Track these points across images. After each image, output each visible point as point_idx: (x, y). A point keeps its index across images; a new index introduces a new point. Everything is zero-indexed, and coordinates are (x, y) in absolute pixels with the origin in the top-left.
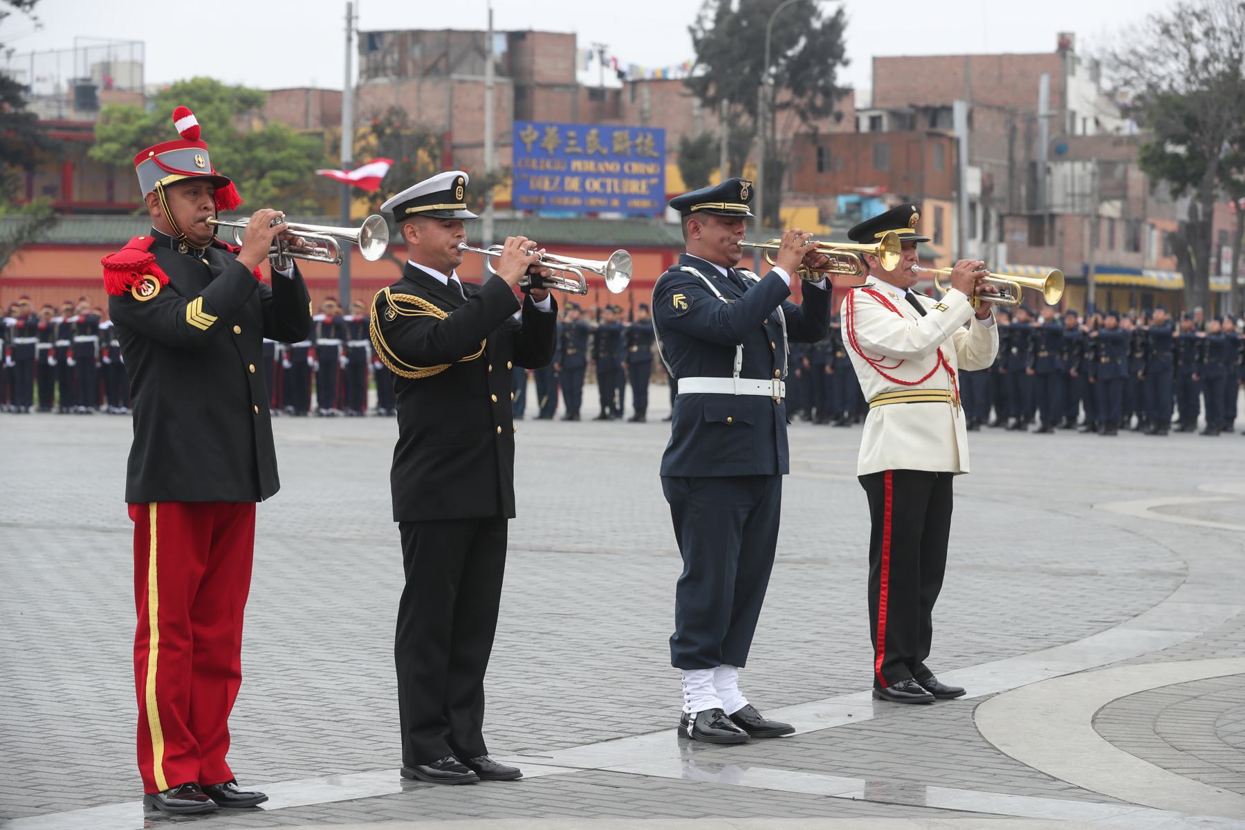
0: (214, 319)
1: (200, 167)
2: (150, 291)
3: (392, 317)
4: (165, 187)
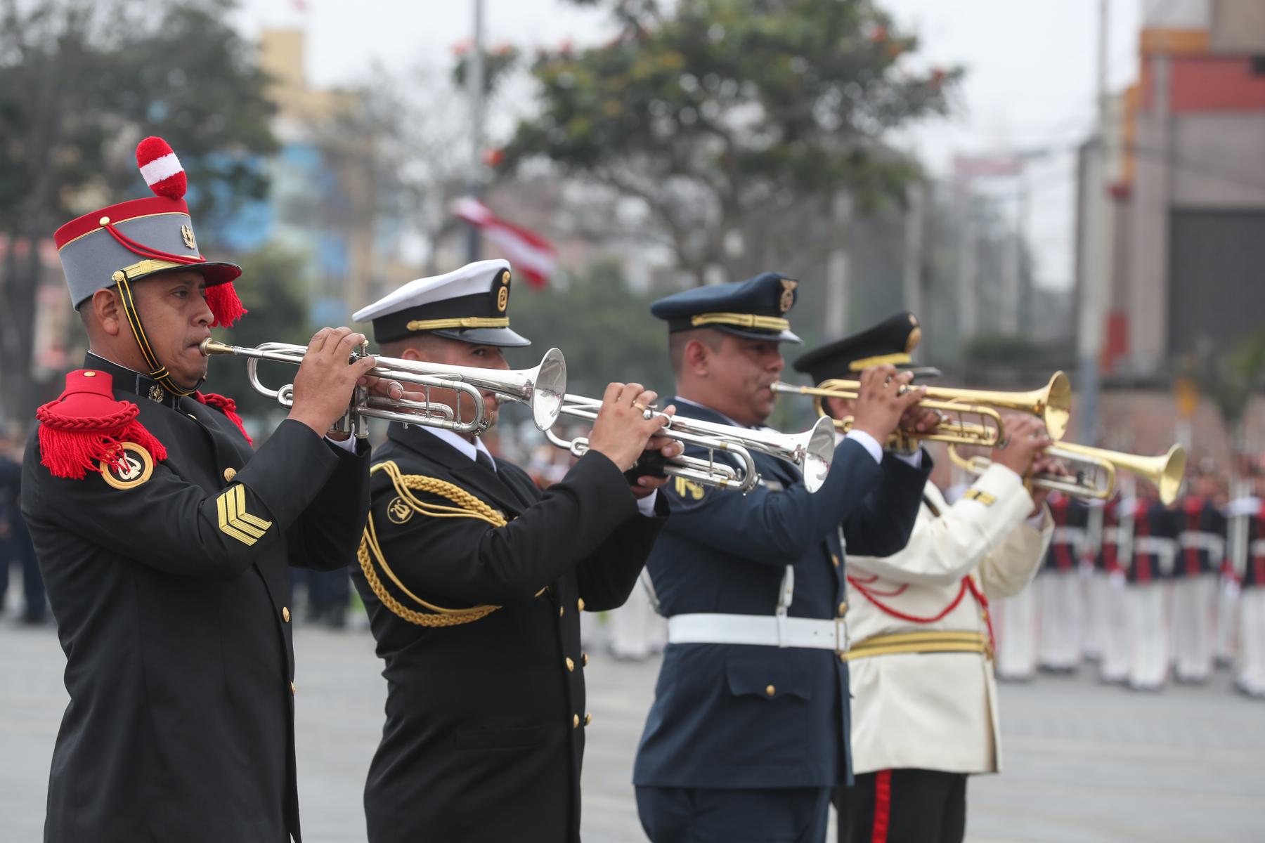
0: (266, 525)
1: (189, 248)
2: (134, 472)
3: (403, 516)
4: (132, 282)
